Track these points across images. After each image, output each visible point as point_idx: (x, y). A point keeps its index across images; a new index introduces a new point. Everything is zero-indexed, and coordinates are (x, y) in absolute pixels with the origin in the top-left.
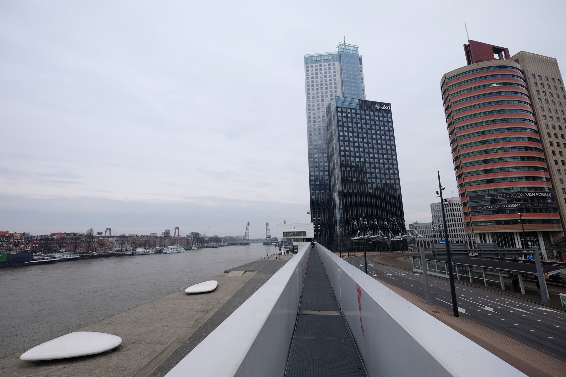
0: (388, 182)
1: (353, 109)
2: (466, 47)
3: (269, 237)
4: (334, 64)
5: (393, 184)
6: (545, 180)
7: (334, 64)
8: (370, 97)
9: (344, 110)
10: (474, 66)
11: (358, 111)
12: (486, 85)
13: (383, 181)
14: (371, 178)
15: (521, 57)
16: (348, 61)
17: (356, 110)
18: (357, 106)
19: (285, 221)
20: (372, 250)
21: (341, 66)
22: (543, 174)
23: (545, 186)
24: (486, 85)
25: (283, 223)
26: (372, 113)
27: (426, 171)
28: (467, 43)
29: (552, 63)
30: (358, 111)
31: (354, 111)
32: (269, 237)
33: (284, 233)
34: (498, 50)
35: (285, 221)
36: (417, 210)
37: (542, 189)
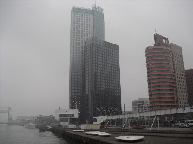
0: (109, 87)
1: (101, 46)
2: (154, 35)
3: (10, 119)
4: (90, 16)
5: (113, 89)
6: (175, 91)
7: (90, 16)
8: (107, 40)
9: (98, 46)
10: (157, 47)
11: (103, 48)
12: (161, 55)
13: (106, 87)
14: (101, 85)
15: (172, 46)
16: (97, 15)
17: (102, 46)
18: (103, 45)
19: (60, 108)
20: (163, 115)
21: (93, 18)
22: (175, 89)
23: (175, 97)
24: (161, 55)
25: (59, 109)
26: (109, 49)
27: (134, 85)
28: (155, 34)
29: (180, 49)
30: (103, 48)
31: (98, 46)
32: (10, 119)
33: (59, 114)
34: (165, 38)
35: (60, 108)
36: (127, 105)
37: (174, 98)
